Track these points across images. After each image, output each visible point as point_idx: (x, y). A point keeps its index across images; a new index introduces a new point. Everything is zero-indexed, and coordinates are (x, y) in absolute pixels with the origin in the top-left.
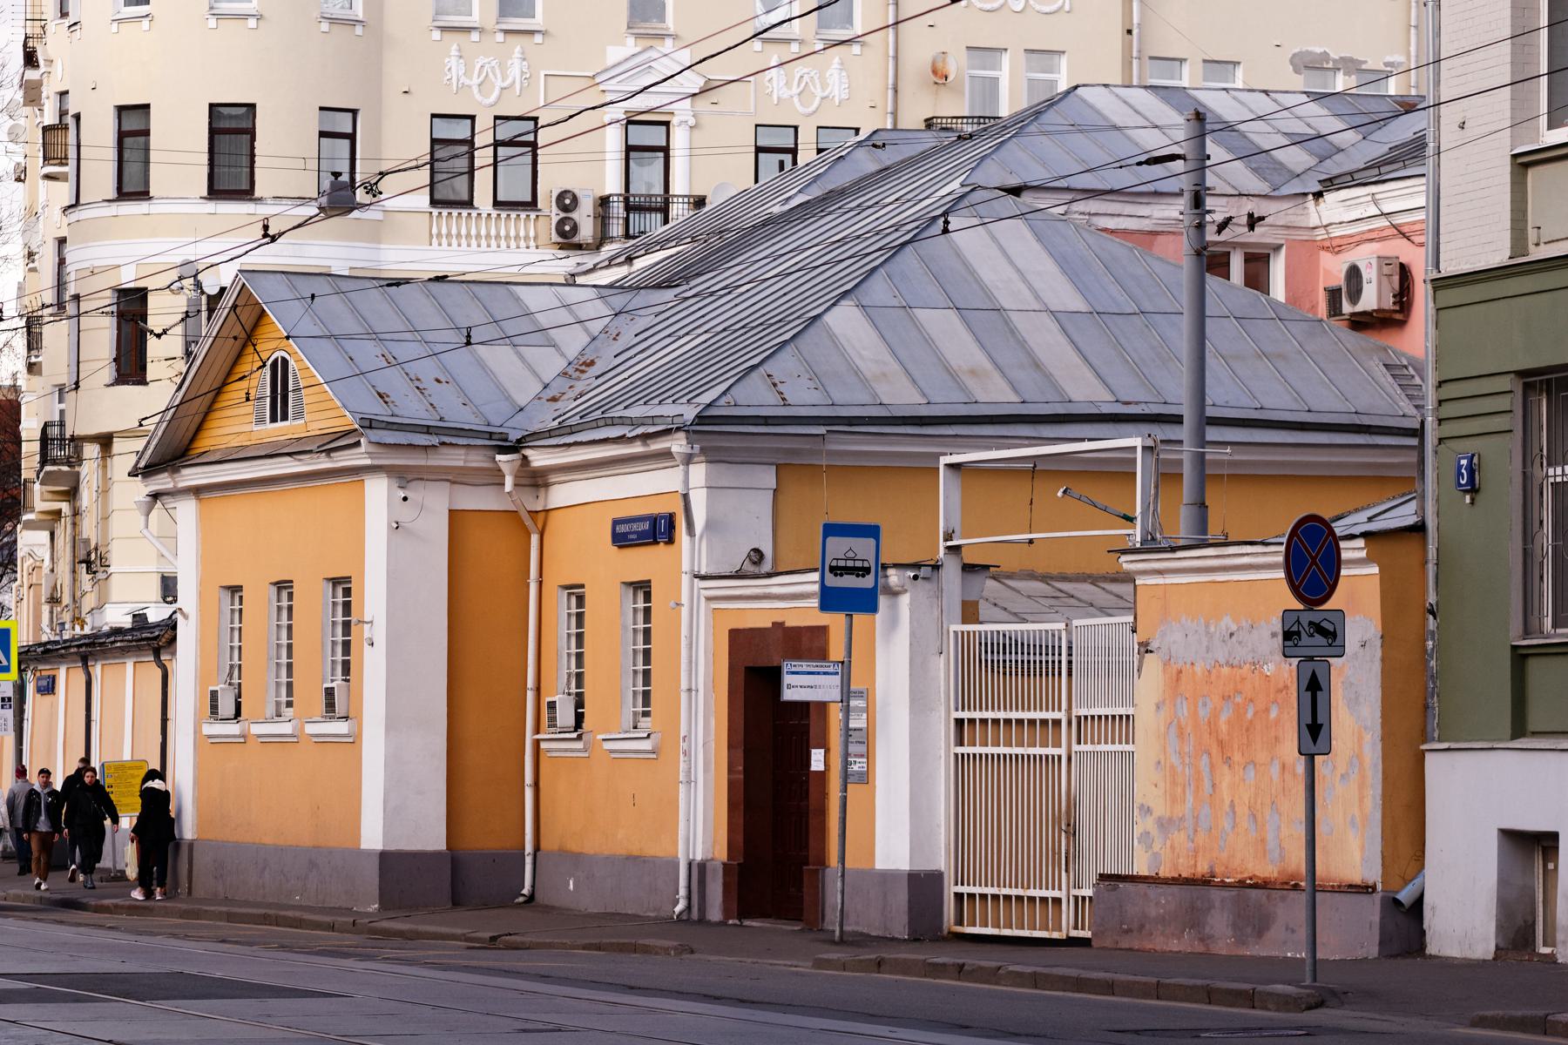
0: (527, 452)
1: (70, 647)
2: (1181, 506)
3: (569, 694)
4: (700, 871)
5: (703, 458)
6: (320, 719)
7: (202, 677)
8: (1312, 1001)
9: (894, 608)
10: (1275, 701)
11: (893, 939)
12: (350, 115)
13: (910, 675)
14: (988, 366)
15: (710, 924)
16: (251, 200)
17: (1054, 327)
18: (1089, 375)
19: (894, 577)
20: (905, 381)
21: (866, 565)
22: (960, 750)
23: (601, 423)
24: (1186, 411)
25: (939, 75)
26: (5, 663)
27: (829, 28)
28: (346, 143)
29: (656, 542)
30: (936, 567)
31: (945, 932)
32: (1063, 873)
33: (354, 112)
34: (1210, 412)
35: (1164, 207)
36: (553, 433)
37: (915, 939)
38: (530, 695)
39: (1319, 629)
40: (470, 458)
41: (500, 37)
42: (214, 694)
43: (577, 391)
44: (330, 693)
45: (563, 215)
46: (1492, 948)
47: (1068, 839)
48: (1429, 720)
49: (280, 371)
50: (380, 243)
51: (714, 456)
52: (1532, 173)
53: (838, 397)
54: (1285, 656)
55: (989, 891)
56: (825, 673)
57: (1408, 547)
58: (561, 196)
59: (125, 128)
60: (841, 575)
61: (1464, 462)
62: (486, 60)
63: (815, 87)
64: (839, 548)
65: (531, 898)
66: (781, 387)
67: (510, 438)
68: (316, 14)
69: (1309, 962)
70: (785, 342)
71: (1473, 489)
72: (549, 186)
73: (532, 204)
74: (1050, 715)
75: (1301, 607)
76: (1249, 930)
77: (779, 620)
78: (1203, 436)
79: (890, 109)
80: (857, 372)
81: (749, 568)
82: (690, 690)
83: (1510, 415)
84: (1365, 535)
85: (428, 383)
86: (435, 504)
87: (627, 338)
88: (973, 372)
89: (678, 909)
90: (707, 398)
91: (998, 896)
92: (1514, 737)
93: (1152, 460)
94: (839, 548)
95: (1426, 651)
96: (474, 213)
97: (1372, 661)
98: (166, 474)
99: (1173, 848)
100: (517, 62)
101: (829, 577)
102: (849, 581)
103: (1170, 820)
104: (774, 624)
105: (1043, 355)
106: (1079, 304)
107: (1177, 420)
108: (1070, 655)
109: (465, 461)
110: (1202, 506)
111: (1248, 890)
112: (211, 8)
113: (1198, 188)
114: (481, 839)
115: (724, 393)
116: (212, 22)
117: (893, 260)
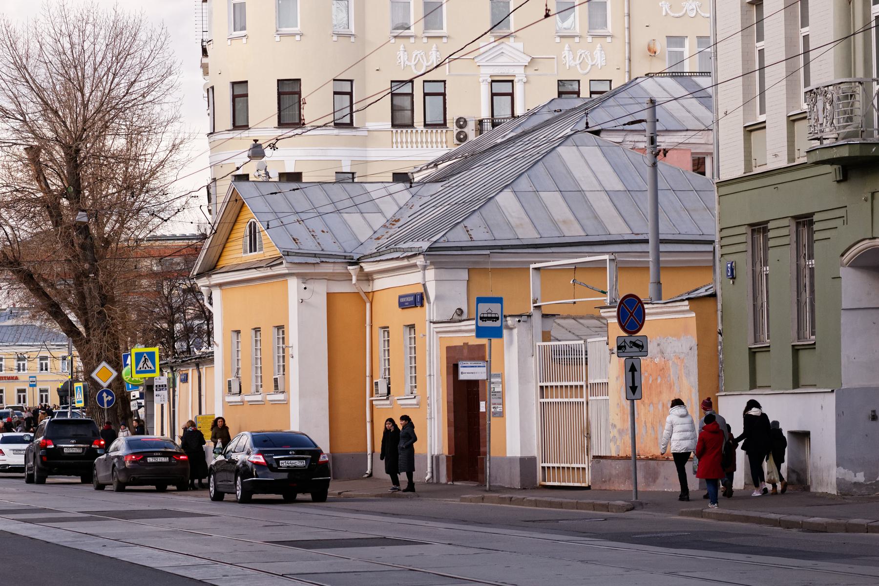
0: (362, 264)
1: (192, 359)
2: (841, 268)
3: (385, 378)
4: (436, 459)
5: (433, 267)
6: (273, 393)
7: (225, 374)
8: (629, 507)
9: (511, 335)
10: (659, 375)
11: (515, 489)
12: (349, 82)
13: (519, 366)
14: (572, 218)
15: (441, 484)
17: (606, 198)
18: (620, 220)
19: (510, 321)
20: (531, 226)
21: (497, 316)
22: (542, 400)
23: (392, 250)
24: (650, 237)
25: (652, 52)
26: (153, 368)
27: (595, 29)
28: (348, 97)
29: (416, 306)
30: (529, 316)
31: (538, 485)
32: (586, 456)
33: (351, 81)
34: (661, 237)
35: (670, 137)
36: (372, 256)
37: (524, 488)
38: (368, 379)
39: (635, 344)
40: (336, 268)
41: (425, 40)
42: (230, 382)
43: (389, 234)
44: (276, 380)
45: (459, 130)
46: (743, 484)
47: (587, 440)
48: (720, 381)
49: (253, 229)
50: (366, 147)
51: (438, 266)
52: (753, 134)
53: (497, 236)
54: (618, 357)
55: (556, 465)
56: (479, 367)
57: (709, 303)
58: (458, 120)
60: (485, 321)
61: (729, 265)
62: (418, 52)
63: (588, 60)
64: (484, 308)
65: (371, 475)
66: (470, 232)
67: (354, 258)
68: (330, 32)
69: (634, 491)
70: (474, 211)
71: (733, 278)
72: (452, 116)
73: (444, 125)
74: (579, 383)
75: (627, 335)
76: (650, 479)
77: (466, 342)
78: (659, 249)
79: (627, 69)
80: (509, 223)
81: (456, 317)
82: (430, 375)
83: (746, 244)
84: (688, 299)
85: (318, 233)
86: (319, 291)
87: (416, 208)
88: (564, 222)
89: (427, 478)
90: (434, 239)
91: (559, 467)
92: (794, 388)
93: (614, 265)
94: (484, 308)
95: (718, 351)
96: (414, 131)
97: (694, 356)
98: (205, 278)
99: (624, 443)
100: (434, 52)
101: (480, 322)
102: (489, 324)
103: (623, 430)
104: (464, 343)
105: (600, 213)
106: (620, 187)
107: (646, 241)
108: (586, 355)
109: (333, 270)
110: (659, 283)
111: (650, 461)
112: (277, 31)
113: (652, 135)
114: (346, 448)
115: (443, 236)
116: (278, 38)
117: (532, 169)
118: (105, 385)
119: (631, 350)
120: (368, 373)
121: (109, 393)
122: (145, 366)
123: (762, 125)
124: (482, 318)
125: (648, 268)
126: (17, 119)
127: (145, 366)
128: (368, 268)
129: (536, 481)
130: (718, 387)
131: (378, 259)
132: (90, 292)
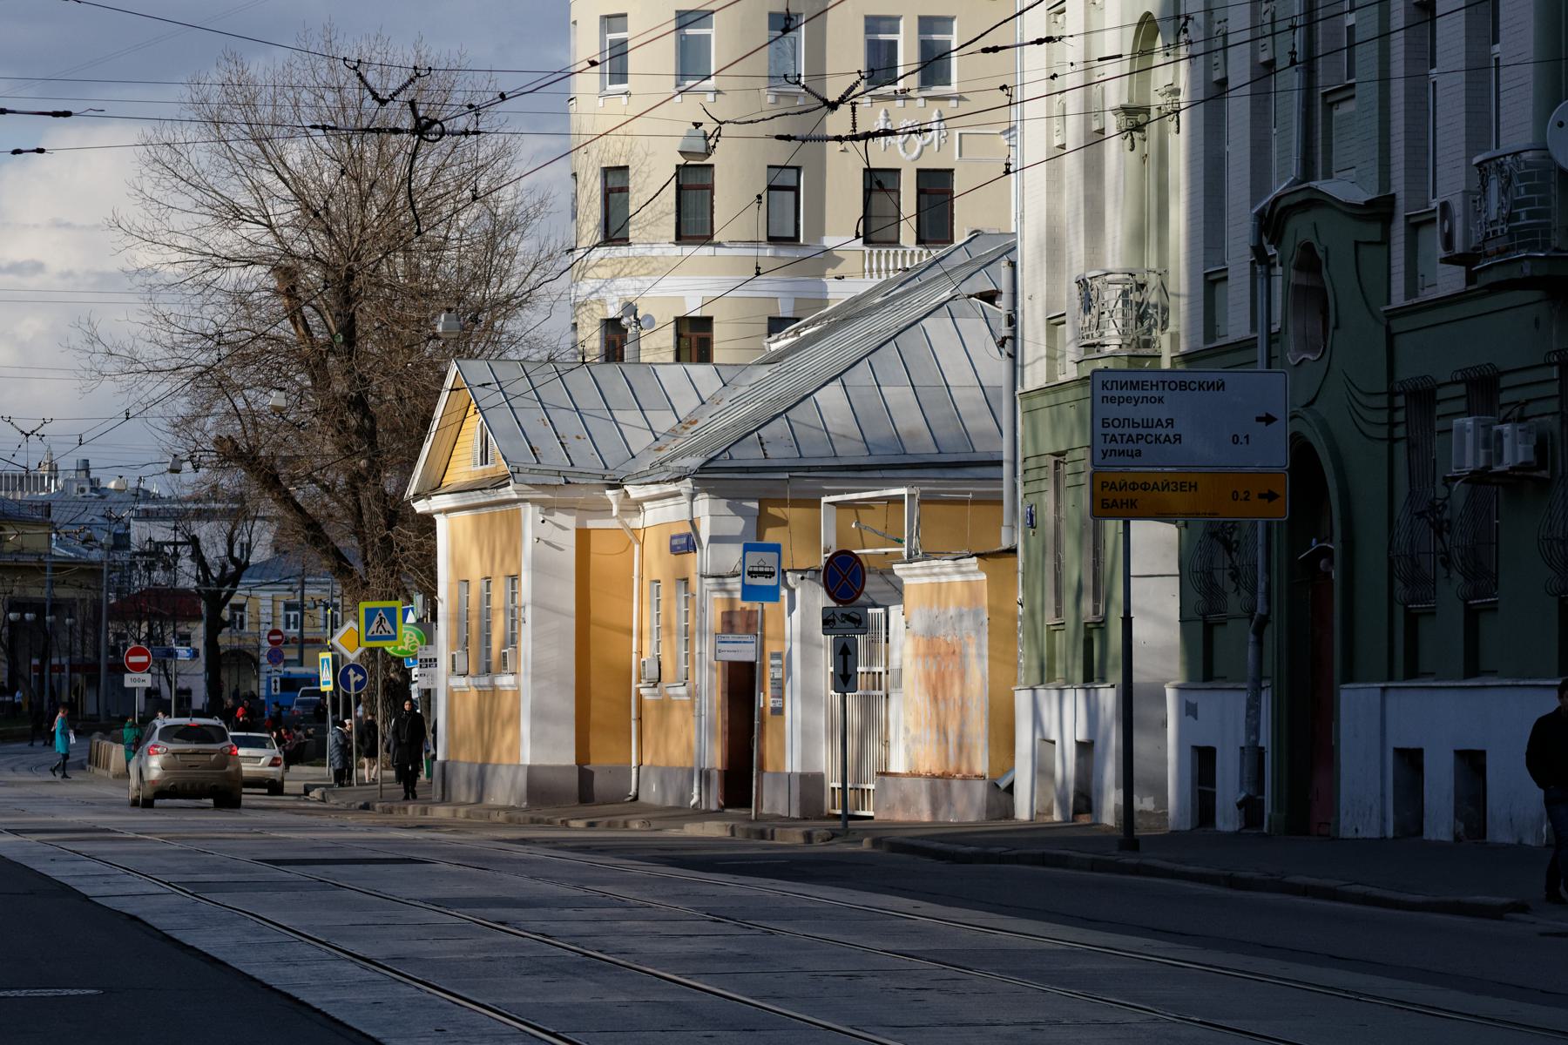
5: (706, 495)
12: (795, 171)
16: (710, 244)
21: (772, 570)
26: (393, 633)
28: (791, 194)
36: (639, 475)
39: (849, 618)
41: (921, 102)
42: (453, 656)
51: (717, 492)
56: (745, 642)
59: (610, 185)
65: (636, 798)
89: (692, 803)
92: (1467, 676)
96: (900, 251)
115: (724, 451)
119: (843, 625)
120: (634, 650)
121: (358, 670)
122: (381, 628)
125: (1000, 503)
126: (258, 223)
127: (381, 628)
129: (823, 807)
130: (1016, 678)
131: (643, 481)
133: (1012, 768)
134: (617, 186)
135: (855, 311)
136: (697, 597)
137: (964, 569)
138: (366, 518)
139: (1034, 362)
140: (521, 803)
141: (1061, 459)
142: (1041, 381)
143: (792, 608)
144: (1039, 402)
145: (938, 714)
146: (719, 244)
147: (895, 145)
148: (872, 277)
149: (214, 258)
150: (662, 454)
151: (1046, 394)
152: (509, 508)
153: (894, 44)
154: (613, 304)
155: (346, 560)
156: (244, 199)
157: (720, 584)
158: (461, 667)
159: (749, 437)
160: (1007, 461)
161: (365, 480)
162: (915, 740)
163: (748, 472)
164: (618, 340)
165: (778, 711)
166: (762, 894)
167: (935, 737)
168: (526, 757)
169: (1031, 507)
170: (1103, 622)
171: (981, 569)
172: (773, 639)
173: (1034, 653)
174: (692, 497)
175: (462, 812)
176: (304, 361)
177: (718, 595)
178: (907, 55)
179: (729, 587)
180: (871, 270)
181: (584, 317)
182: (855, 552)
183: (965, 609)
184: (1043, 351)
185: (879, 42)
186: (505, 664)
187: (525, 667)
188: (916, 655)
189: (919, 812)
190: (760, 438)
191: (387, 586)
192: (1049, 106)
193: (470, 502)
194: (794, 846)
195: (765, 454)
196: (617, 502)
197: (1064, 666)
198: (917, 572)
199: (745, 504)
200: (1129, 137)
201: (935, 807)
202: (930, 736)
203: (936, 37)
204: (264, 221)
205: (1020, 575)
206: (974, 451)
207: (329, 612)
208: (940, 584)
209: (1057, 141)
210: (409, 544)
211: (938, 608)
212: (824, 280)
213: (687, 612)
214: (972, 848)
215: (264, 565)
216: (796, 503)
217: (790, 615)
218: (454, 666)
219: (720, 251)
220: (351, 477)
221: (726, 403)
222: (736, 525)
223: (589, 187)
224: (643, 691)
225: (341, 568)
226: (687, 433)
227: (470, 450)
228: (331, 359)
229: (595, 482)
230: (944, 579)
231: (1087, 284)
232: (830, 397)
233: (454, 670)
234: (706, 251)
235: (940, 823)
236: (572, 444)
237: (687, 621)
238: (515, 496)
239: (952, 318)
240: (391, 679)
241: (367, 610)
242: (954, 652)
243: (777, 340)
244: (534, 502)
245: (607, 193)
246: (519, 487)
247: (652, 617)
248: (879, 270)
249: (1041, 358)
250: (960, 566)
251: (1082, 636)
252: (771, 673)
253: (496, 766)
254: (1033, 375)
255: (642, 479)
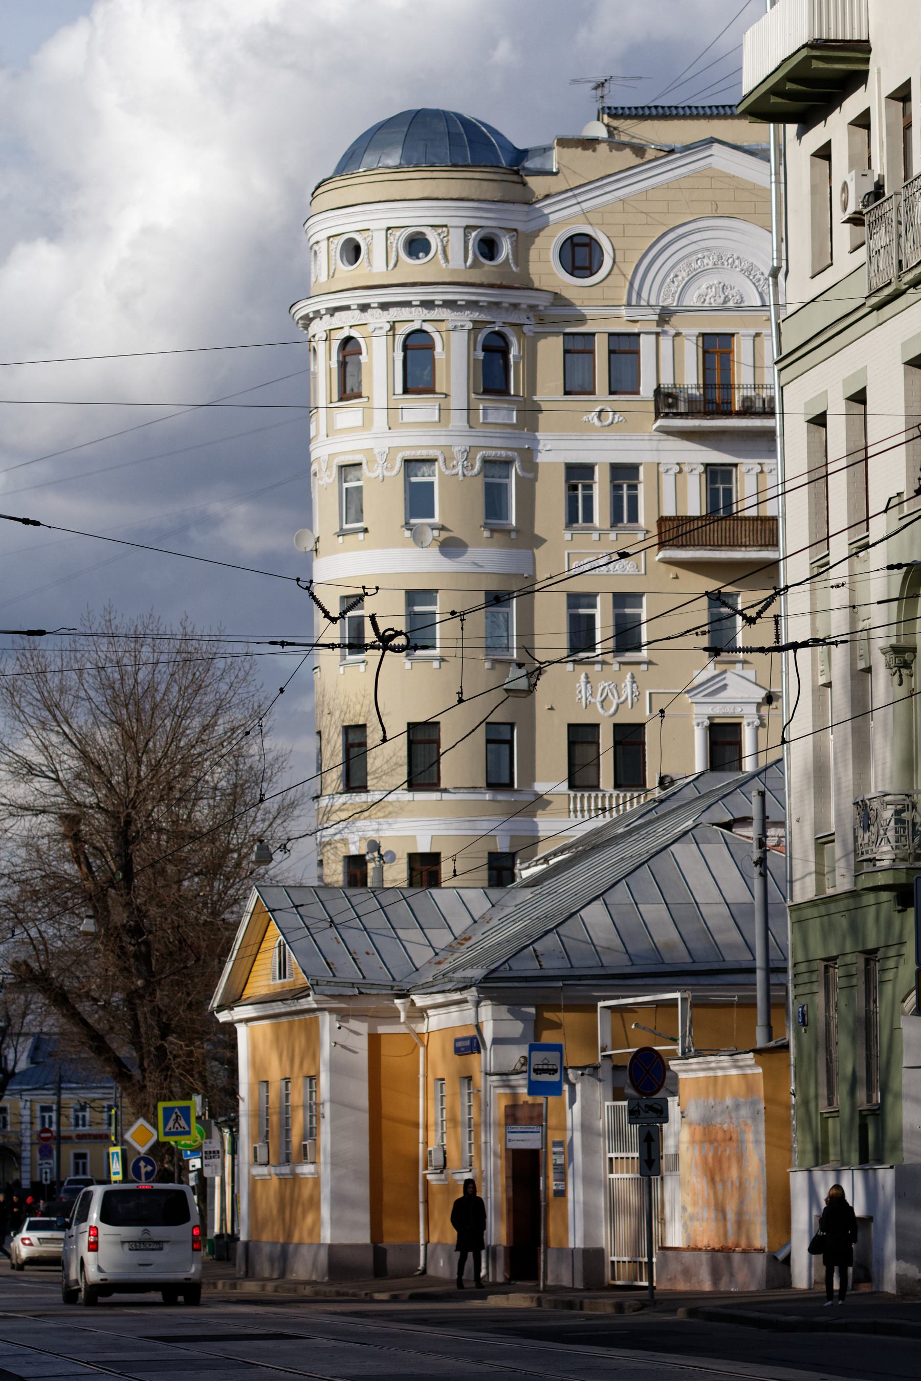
0: (413, 997)
5: (489, 1002)
26: (187, 1129)
34: (771, 965)
42: (255, 1148)
59: (350, 741)
65: (424, 1271)
82: (486, 1143)
96: (600, 794)
118: (143, 1150)
119: (647, 1115)
120: (421, 1140)
121: (148, 1162)
122: (177, 1125)
123: (831, 838)
124: (537, 1071)
125: (754, 1005)
128: (420, 1001)
130: (790, 1161)
131: (430, 990)
132: (146, 1018)
133: (789, 1242)
134: (356, 741)
135: (600, 840)
136: (482, 1093)
137: (741, 1064)
138: (142, 1030)
139: (803, 877)
140: (323, 1278)
141: (830, 963)
142: (810, 894)
143: (572, 1101)
144: (809, 912)
145: (715, 1194)
146: (445, 790)
147: (595, 703)
148: (576, 817)
149: (10, 808)
150: (442, 967)
151: (816, 905)
152: (307, 1016)
153: (592, 617)
154: (354, 843)
155: (125, 1067)
156: (37, 759)
157: (503, 1081)
158: (262, 1157)
159: (525, 951)
160: (760, 968)
161: (142, 997)
162: (691, 1218)
163: (526, 981)
164: (358, 874)
165: (561, 1194)
166: (660, 1367)
167: (713, 1215)
168: (327, 1236)
169: (803, 1007)
170: (879, 1109)
171: (758, 1063)
172: (556, 1129)
173: (808, 1139)
174: (477, 1004)
175: (270, 1286)
176: (89, 898)
177: (501, 1091)
178: (603, 629)
179: (513, 1083)
180: (575, 811)
181: (329, 854)
182: (656, 1048)
183: (742, 1100)
184: (812, 867)
185: (580, 616)
186: (305, 1155)
187: (324, 1157)
188: (693, 1142)
189: (700, 1282)
190: (535, 951)
191: (162, 1088)
192: (898, 629)
193: (271, 1012)
194: (607, 1317)
195: (541, 965)
196: (405, 1011)
197: (839, 1149)
198: (694, 1067)
199: (524, 1009)
200: (898, 674)
201: (716, 1275)
202: (708, 1214)
203: (628, 611)
204: (52, 775)
205: (792, 1068)
206: (724, 960)
207: (113, 1112)
208: (716, 1077)
209: (822, 680)
210: (181, 1052)
211: (715, 1099)
212: (535, 820)
213: (470, 1106)
214: (793, 1317)
215: (23, 1073)
216: (569, 1008)
217: (571, 1107)
218: (256, 1157)
219: (446, 796)
220: (128, 995)
221: (495, 922)
222: (516, 1028)
223: (332, 743)
224: (429, 1177)
225: (122, 1073)
226: (463, 949)
227: (269, 966)
228: (112, 892)
229: (384, 992)
230: (720, 1073)
231: (866, 805)
232: (595, 914)
233: (256, 1161)
234: (434, 796)
235: (721, 1292)
236: (361, 958)
237: (470, 1114)
238: (315, 1006)
239: (697, 844)
240: (166, 1170)
241: (165, 1109)
242: (731, 1139)
243: (528, 868)
244: (331, 1011)
245: (348, 747)
246: (318, 997)
247: (436, 1112)
248: (582, 811)
249: (810, 873)
250: (736, 1061)
251: (857, 1121)
252: (554, 1159)
253: (299, 1244)
254: (803, 888)
255: (427, 989)
